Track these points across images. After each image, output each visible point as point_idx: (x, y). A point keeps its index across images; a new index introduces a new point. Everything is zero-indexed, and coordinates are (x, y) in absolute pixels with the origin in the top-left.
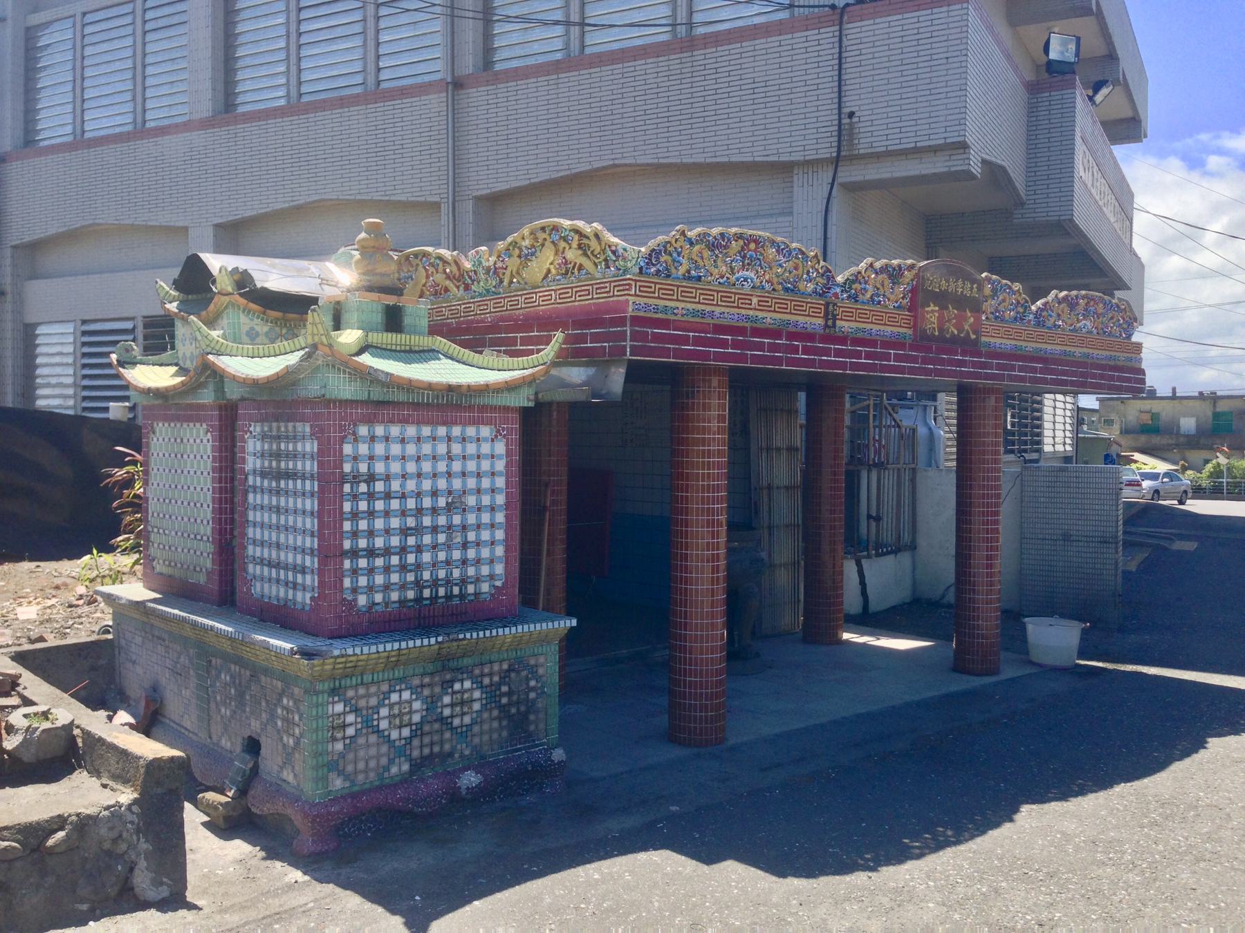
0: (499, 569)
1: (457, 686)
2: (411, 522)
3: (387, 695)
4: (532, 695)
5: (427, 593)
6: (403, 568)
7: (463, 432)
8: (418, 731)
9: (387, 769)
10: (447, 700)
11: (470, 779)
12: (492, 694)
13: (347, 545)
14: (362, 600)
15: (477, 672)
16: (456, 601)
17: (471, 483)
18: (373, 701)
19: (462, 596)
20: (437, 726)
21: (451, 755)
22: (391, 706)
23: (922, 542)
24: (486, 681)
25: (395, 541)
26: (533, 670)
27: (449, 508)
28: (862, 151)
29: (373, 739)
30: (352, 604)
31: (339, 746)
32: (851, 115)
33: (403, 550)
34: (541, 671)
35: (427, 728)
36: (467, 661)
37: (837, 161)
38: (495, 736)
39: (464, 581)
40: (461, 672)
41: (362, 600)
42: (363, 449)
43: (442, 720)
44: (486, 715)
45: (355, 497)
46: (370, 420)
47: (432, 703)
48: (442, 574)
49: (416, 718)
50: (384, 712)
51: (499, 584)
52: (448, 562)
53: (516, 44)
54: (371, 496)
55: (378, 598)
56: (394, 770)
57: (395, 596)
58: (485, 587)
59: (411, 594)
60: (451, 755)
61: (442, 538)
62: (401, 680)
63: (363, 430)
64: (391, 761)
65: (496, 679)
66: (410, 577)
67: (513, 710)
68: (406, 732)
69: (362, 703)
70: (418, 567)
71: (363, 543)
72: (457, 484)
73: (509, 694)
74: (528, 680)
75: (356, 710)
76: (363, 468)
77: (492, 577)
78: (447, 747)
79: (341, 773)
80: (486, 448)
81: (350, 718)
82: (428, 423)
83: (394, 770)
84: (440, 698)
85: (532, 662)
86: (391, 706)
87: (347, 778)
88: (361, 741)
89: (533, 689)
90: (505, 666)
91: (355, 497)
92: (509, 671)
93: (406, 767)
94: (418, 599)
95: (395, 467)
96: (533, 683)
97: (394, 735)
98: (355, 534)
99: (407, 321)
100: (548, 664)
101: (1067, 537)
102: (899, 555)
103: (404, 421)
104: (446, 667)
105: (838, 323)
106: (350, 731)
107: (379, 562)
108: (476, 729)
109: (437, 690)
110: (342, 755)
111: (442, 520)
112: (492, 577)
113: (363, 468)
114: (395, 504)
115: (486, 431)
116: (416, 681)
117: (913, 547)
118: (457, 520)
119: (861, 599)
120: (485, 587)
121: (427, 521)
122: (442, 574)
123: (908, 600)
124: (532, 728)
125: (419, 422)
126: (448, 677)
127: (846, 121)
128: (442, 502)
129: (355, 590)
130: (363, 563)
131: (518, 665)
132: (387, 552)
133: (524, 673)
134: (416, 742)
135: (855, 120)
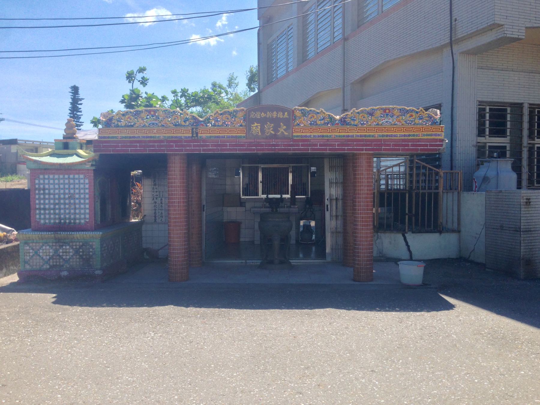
0: (87, 216)
1: (64, 247)
2: (57, 201)
3: (42, 247)
4: (91, 253)
5: (62, 221)
6: (55, 214)
7: (74, 176)
8: (51, 258)
9: (43, 266)
10: (61, 251)
11: (65, 273)
12: (77, 252)
13: (37, 206)
14: (42, 221)
15: (71, 244)
16: (72, 224)
17: (77, 191)
18: (38, 248)
19: (75, 223)
20: (58, 257)
21: (63, 266)
22: (43, 250)
23: (463, 229)
24: (74, 247)
25: (52, 206)
26: (91, 246)
27: (69, 198)
28: (459, 37)
29: (38, 257)
30: (38, 222)
31: (28, 258)
32: (456, 20)
33: (54, 209)
34: (94, 247)
35: (54, 257)
36: (67, 241)
37: (451, 44)
38: (78, 263)
39: (75, 219)
40: (65, 243)
41: (42, 221)
42: (42, 181)
43: (59, 255)
44: (74, 257)
45: (39, 194)
46: (44, 174)
47: (56, 251)
48: (67, 216)
49: (51, 254)
50: (41, 251)
51: (88, 220)
52: (69, 213)
53: (371, 10)
54: (44, 194)
55: (47, 221)
56: (45, 267)
57: (52, 221)
58: (83, 221)
59: (57, 221)
60: (63, 266)
61: (67, 206)
62: (46, 243)
63: (41, 177)
64: (44, 264)
65: (78, 247)
66: (57, 216)
67: (84, 257)
68: (48, 257)
69: (34, 248)
70: (59, 214)
71: (42, 206)
72: (72, 191)
73: (83, 252)
74: (89, 249)
75: (33, 249)
76: (42, 186)
77: (85, 218)
78: (61, 264)
79: (29, 264)
80: (82, 181)
81: (31, 251)
82: (61, 174)
83: (45, 267)
84: (59, 250)
85: (91, 244)
86: (43, 250)
87: (30, 266)
88: (34, 257)
89: (91, 252)
90: (81, 244)
91: (39, 194)
92: (82, 245)
93: (48, 267)
94: (60, 223)
95: (52, 186)
96: (91, 250)
97: (44, 257)
98: (40, 204)
99: (70, 146)
100: (96, 245)
101: (502, 227)
102: (443, 235)
103: (54, 174)
104: (60, 242)
105: (199, 135)
106: (31, 254)
107: (47, 212)
108: (71, 260)
109: (58, 247)
110: (29, 260)
111: (67, 201)
112: (85, 218)
113: (42, 186)
114: (52, 196)
115: (82, 176)
116: (51, 244)
117: (459, 232)
118: (72, 201)
119: (408, 253)
120: (83, 221)
121: (62, 201)
122: (67, 216)
123: (454, 256)
124: (91, 263)
125: (59, 174)
126: (61, 244)
127: (454, 23)
128: (67, 196)
129: (40, 218)
130: (42, 212)
131: (85, 244)
132: (50, 209)
133: (88, 247)
134: (51, 261)
135: (457, 22)
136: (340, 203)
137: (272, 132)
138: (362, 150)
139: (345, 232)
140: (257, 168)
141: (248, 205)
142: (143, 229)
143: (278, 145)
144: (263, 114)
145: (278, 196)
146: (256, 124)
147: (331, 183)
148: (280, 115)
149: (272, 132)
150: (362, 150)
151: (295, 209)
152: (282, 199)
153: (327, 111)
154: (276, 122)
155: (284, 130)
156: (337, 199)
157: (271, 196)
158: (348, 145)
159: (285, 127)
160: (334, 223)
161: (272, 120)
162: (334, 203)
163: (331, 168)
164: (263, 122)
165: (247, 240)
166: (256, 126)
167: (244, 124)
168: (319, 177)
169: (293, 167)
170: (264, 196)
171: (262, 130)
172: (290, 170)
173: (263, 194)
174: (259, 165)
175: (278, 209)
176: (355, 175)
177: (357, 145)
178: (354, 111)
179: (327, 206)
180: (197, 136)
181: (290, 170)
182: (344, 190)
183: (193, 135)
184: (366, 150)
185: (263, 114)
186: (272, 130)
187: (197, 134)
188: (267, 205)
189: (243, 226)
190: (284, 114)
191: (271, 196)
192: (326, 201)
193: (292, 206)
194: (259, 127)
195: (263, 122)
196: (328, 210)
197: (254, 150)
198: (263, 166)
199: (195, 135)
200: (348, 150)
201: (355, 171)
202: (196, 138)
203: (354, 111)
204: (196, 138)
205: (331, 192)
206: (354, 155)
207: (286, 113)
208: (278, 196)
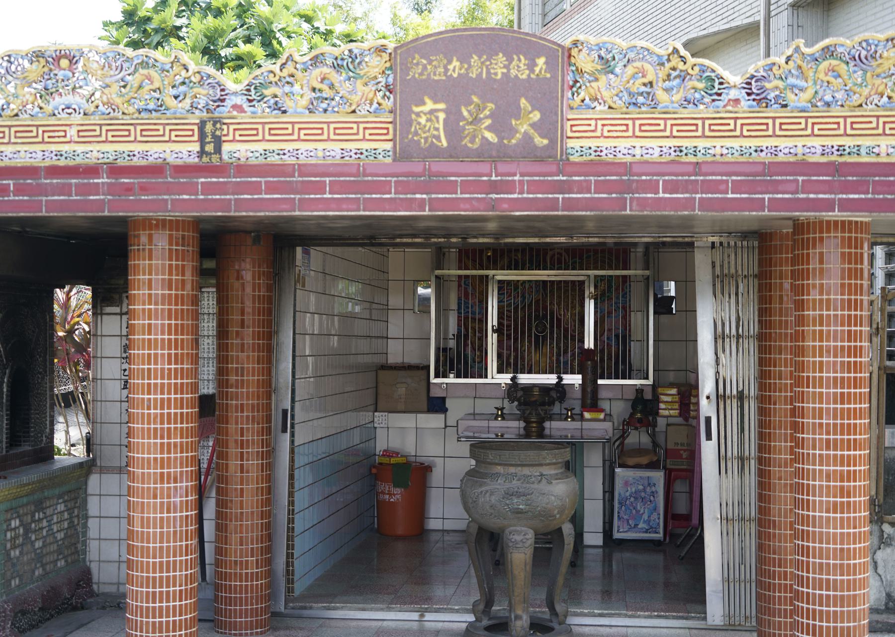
105: (226, 148)
136: (751, 407)
137: (490, 136)
138: (829, 205)
139: (764, 519)
140: (484, 280)
141: (456, 408)
142: (90, 490)
143: (509, 187)
144: (456, 63)
145: (551, 379)
146: (430, 105)
147: (719, 337)
148: (520, 69)
149: (490, 136)
150: (829, 205)
151: (597, 426)
152: (560, 389)
153: (693, 55)
154: (505, 97)
155: (533, 125)
156: (741, 396)
157: (525, 379)
158: (774, 187)
159: (536, 116)
160: (732, 481)
161: (488, 88)
162: (733, 407)
163: (722, 282)
164: (453, 93)
165: (449, 525)
166: (432, 112)
167: (413, 116)
168: (676, 316)
169: (598, 280)
170: (505, 379)
171: (453, 129)
172: (590, 290)
173: (500, 371)
174: (491, 273)
175: (547, 424)
176: (800, 305)
177: (807, 187)
178: (797, 49)
179: (708, 420)
180: (218, 150)
181: (590, 290)
182: (761, 362)
183: (202, 147)
184: (845, 205)
185: (456, 63)
186: (488, 128)
187: (218, 142)
188: (511, 407)
189: (436, 477)
190: (531, 66)
191: (525, 379)
192: (703, 402)
193: (587, 415)
194: (442, 116)
195: (453, 93)
196: (709, 437)
197: (421, 204)
198: (502, 275)
199: (209, 148)
200: (775, 204)
201: (799, 290)
202: (215, 159)
203: (797, 49)
204: (215, 159)
205: (717, 364)
206: (799, 227)
207: (541, 61)
208: (551, 379)
